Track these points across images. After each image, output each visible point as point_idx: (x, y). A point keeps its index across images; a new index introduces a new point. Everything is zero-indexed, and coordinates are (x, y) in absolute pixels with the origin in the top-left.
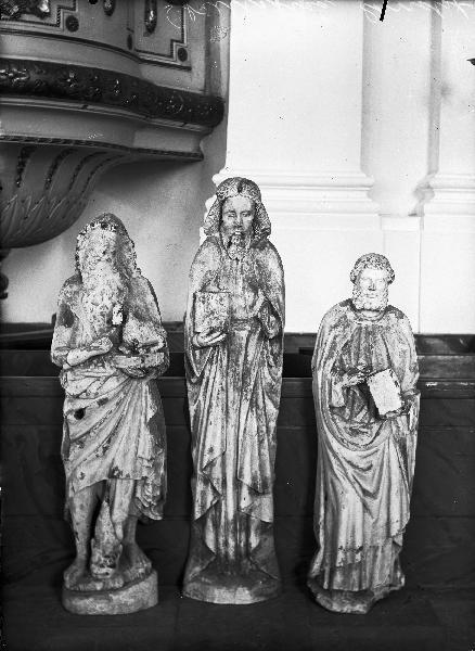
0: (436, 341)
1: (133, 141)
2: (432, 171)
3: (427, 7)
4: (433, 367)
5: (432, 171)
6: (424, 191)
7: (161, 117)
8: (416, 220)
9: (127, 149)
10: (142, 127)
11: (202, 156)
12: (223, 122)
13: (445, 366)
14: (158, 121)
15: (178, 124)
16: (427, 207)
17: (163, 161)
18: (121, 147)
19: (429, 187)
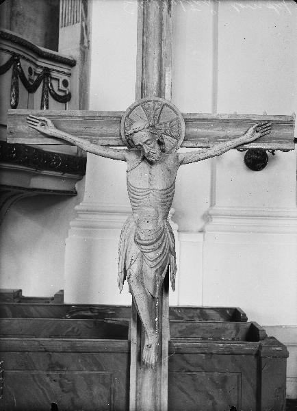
0: (212, 312)
1: (29, 184)
2: (212, 204)
3: (210, 5)
4: (196, 331)
5: (212, 204)
6: (207, 217)
7: (46, 170)
8: (202, 234)
9: (24, 189)
10: (36, 175)
11: (76, 193)
12: (258, 330)
13: (204, 330)
14: (45, 172)
15: (59, 174)
16: (208, 227)
17: (50, 195)
18: (20, 188)
19: (209, 214)
